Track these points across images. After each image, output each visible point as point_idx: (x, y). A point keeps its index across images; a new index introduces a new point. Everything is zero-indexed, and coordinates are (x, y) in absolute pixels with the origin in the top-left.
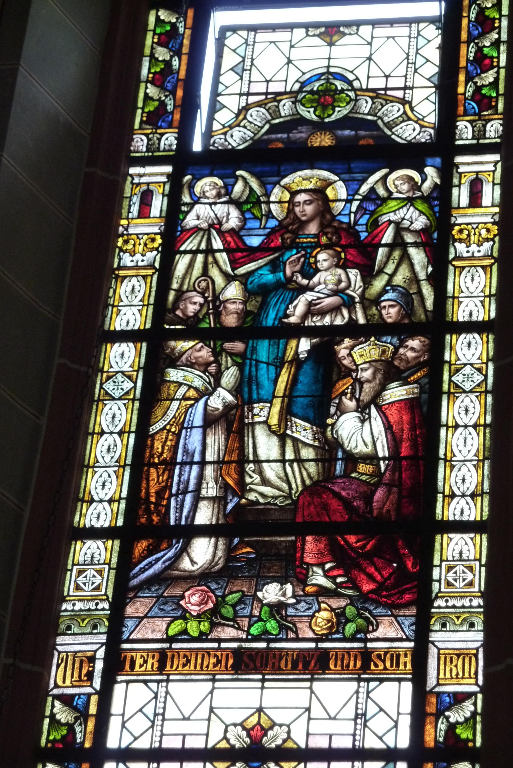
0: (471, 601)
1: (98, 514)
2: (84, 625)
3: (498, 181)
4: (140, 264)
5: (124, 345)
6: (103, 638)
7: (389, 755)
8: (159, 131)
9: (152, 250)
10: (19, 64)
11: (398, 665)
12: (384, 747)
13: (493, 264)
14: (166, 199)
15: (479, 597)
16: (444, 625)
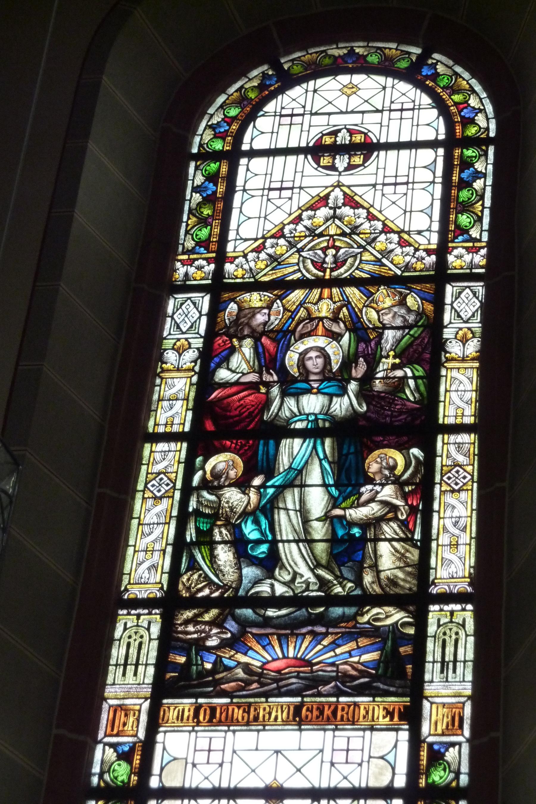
7: (388, 792)
10: (74, 211)
12: (351, 786)
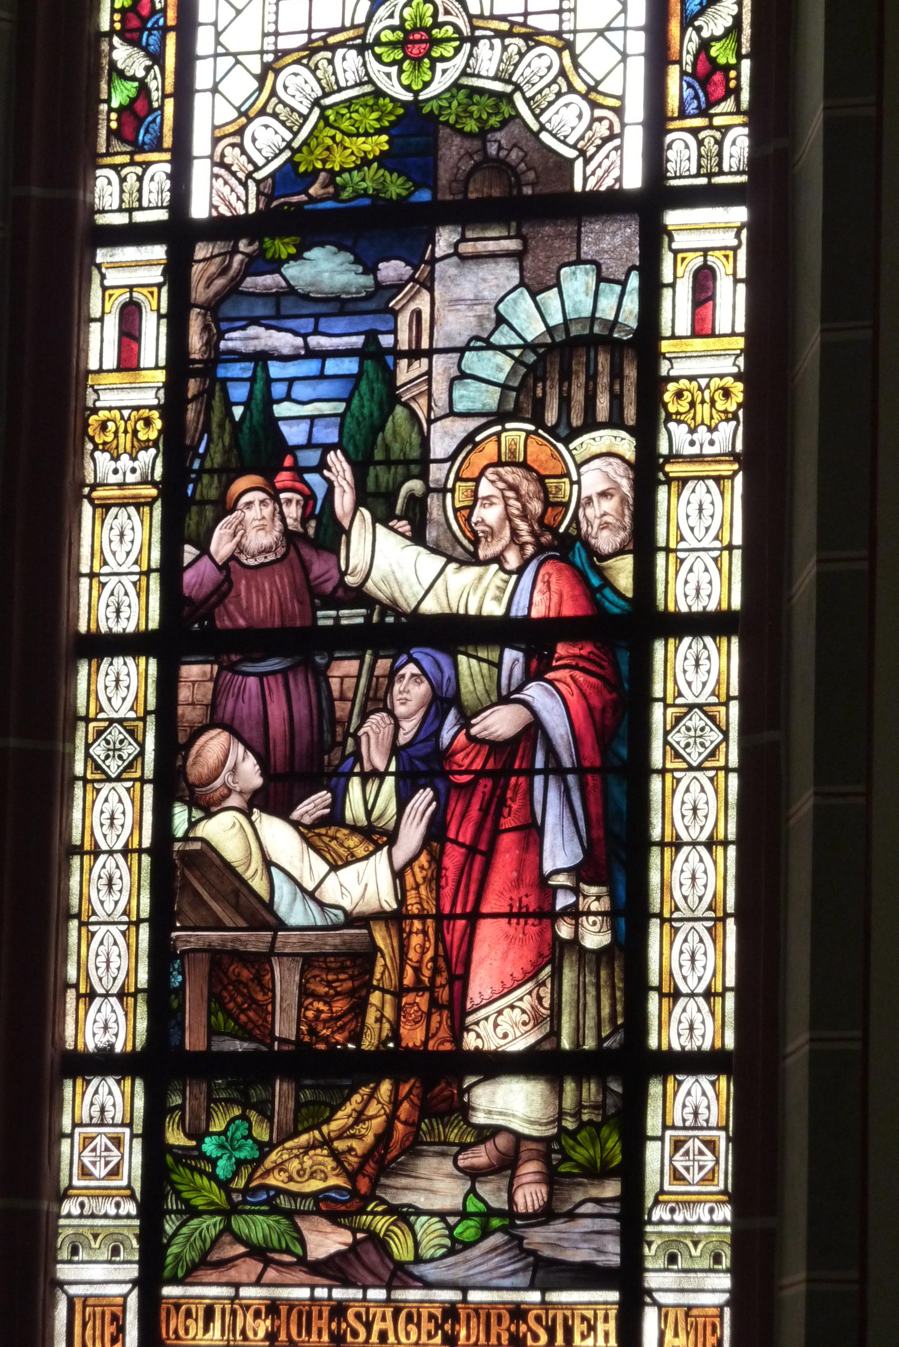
0: (711, 1211)
1: (104, 1024)
2: (97, 1246)
3: (742, 273)
4: (708, 450)
5: (118, 661)
6: (133, 1271)
8: (138, 158)
9: (145, 446)
11: (309, 1333)
13: (735, 473)
14: (164, 322)
15: (723, 1202)
16: (672, 1259)
